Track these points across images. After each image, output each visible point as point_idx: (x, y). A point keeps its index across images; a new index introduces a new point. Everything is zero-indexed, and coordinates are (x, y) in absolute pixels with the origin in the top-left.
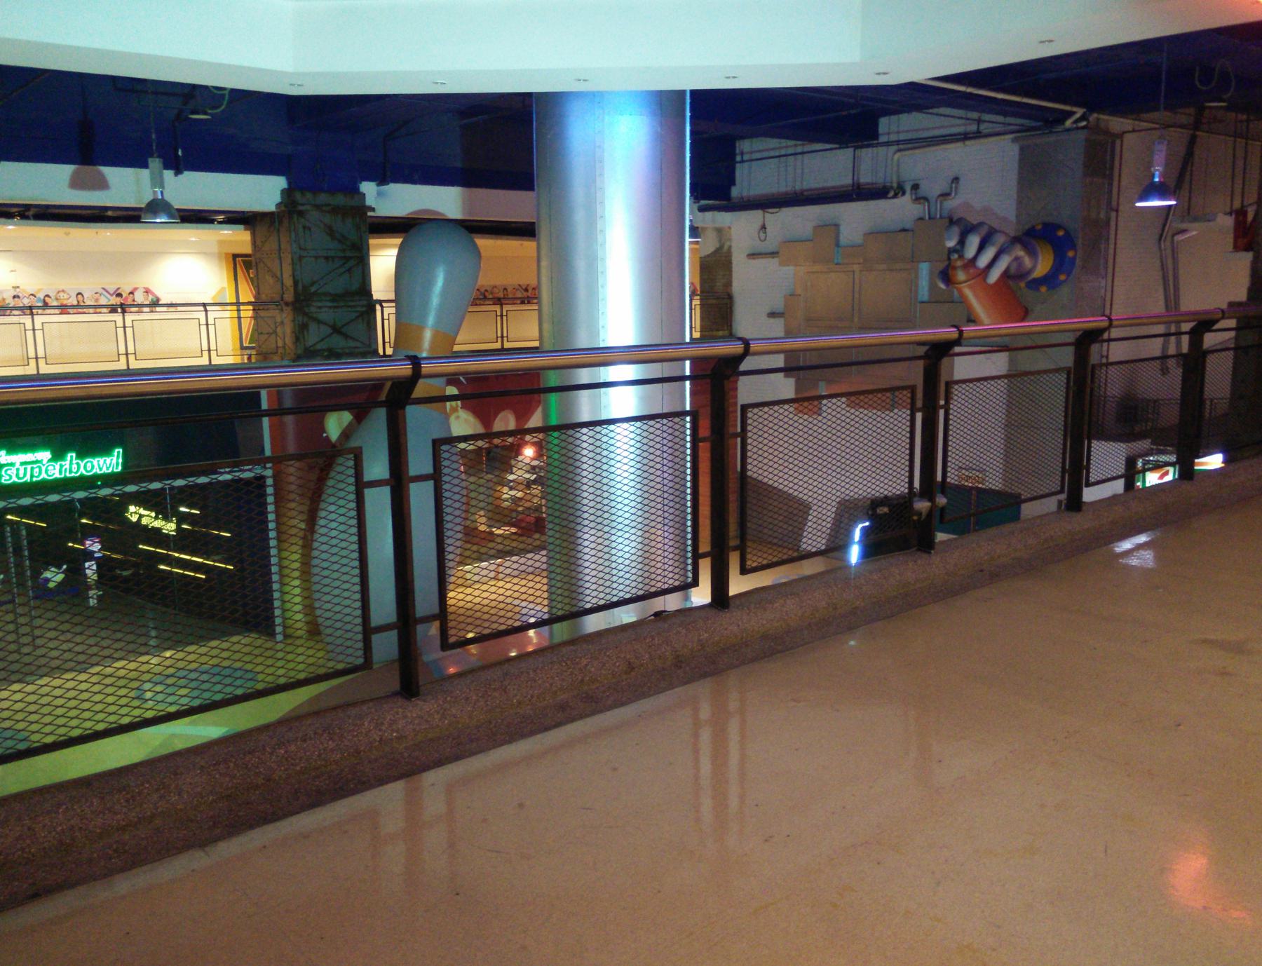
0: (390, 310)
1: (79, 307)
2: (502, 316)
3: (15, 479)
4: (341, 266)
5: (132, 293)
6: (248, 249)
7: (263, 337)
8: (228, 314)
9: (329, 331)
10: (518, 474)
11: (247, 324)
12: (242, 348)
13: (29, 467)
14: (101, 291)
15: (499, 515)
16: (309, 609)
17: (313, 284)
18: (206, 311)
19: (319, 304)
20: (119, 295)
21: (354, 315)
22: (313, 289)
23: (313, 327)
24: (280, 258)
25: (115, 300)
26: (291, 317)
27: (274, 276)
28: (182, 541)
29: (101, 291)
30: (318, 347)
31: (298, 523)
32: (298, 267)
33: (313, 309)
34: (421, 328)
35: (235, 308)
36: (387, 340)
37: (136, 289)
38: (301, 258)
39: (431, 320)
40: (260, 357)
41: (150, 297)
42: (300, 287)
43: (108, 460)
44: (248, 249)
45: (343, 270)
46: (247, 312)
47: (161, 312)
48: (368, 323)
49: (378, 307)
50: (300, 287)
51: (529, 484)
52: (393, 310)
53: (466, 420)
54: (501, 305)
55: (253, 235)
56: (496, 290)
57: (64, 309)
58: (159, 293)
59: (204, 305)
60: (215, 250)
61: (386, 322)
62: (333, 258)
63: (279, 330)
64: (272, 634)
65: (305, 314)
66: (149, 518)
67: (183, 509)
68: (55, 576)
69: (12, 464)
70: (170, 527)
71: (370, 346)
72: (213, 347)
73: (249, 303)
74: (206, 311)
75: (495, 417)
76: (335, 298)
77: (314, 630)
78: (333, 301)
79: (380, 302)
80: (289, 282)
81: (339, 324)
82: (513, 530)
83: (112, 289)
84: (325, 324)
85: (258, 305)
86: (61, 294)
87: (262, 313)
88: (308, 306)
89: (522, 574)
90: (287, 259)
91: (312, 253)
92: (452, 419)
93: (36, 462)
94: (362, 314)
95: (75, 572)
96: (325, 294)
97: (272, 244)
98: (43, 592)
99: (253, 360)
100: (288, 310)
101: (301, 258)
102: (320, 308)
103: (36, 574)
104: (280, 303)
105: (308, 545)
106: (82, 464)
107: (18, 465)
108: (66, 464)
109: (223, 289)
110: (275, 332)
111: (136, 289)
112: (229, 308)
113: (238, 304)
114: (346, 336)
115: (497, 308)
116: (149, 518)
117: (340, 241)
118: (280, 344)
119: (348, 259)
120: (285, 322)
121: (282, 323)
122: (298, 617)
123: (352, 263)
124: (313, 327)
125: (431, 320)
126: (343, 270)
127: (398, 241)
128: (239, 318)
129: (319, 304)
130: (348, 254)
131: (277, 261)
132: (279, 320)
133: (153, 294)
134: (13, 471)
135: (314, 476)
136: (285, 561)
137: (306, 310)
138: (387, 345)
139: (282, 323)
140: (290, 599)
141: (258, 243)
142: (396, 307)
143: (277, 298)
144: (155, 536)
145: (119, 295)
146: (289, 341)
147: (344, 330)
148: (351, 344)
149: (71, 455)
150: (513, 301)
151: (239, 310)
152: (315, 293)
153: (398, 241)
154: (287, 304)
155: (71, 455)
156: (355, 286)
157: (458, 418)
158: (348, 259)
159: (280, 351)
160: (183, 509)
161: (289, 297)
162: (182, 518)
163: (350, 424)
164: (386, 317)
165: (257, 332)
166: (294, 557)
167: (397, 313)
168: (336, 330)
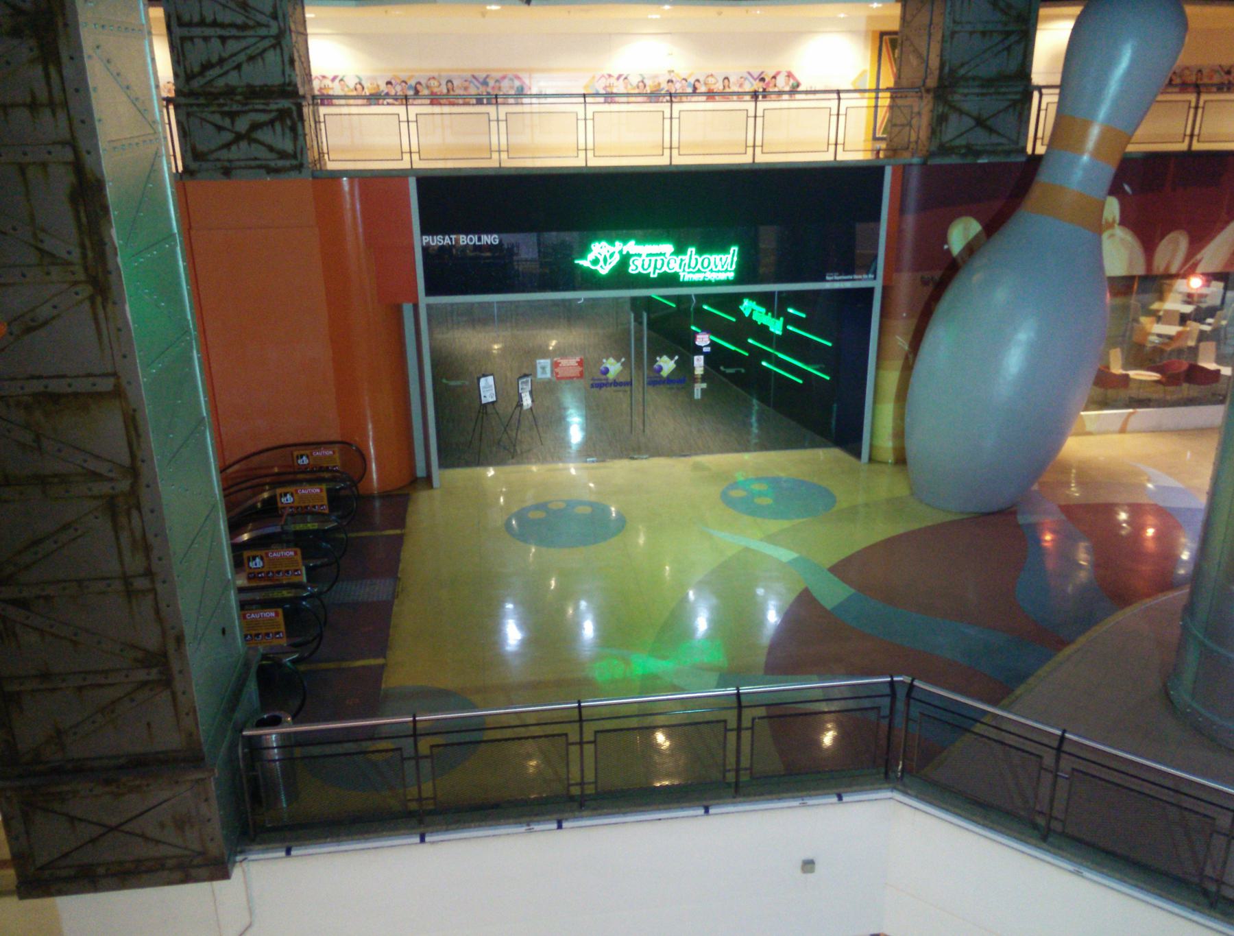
0: (1051, 99)
1: (725, 95)
2: (1197, 108)
3: (640, 270)
4: (1002, 41)
5: (774, 77)
6: (895, 26)
7: (896, 129)
8: (864, 103)
9: (971, 123)
10: (1173, 304)
11: (883, 113)
12: (875, 139)
13: (653, 259)
14: (471, 79)
15: (1140, 355)
16: (900, 434)
17: (962, 65)
18: (839, 99)
19: (966, 91)
20: (763, 80)
21: (1006, 104)
22: (962, 72)
23: (953, 117)
24: (930, 35)
25: (759, 86)
26: (930, 107)
27: (920, 56)
28: (787, 342)
29: (471, 79)
30: (957, 142)
31: (901, 342)
32: (948, 45)
33: (957, 97)
34: (1087, 124)
35: (873, 95)
36: (1040, 134)
37: (778, 73)
38: (953, 33)
39: (1103, 113)
40: (890, 153)
41: (792, 81)
42: (947, 69)
43: (724, 256)
44: (895, 26)
45: (1000, 47)
46: (885, 101)
47: (800, 102)
48: (1020, 114)
49: (1036, 94)
50: (947, 69)
51: (1183, 319)
52: (1056, 99)
53: (1122, 240)
54: (1199, 93)
55: (904, 7)
56: (434, 83)
57: (711, 95)
58: (800, 77)
59: (838, 92)
60: (862, 26)
61: (1042, 114)
62: (991, 32)
63: (914, 122)
64: (857, 454)
65: (947, 103)
66: (761, 315)
67: (791, 310)
68: (667, 365)
69: (639, 255)
70: (776, 326)
71: (1017, 143)
72: (840, 140)
73: (888, 89)
74: (839, 99)
75: (1163, 237)
76: (988, 83)
77: (901, 460)
78: (982, 86)
79: (1039, 88)
80: (934, 62)
81: (985, 115)
82: (1154, 376)
83: (756, 74)
84: (968, 115)
85: (896, 92)
86: (710, 79)
87: (900, 102)
88: (1161, 298)
89: (1157, 430)
90: (937, 36)
91: (969, 28)
92: (1105, 236)
93: (660, 254)
94: (1014, 104)
95: (685, 366)
96: (974, 78)
97: (923, 18)
98: (657, 380)
99: (881, 155)
100: (929, 98)
101: (953, 33)
102: (965, 95)
103: (652, 361)
104: (921, 89)
105: (908, 368)
106: (700, 260)
107: (644, 257)
108: (686, 258)
109: (864, 72)
110: (910, 124)
111: (778, 73)
112: (867, 95)
113: (877, 90)
114: (991, 130)
115: (1192, 98)
116: (761, 315)
117: (1002, 11)
118: (913, 138)
119: (1008, 34)
120: (924, 108)
121: (919, 114)
122: (886, 442)
123: (1013, 38)
124: (953, 117)
125: (1103, 113)
126: (1000, 47)
127: (1077, 10)
128: (876, 107)
129: (966, 91)
130: (1011, 28)
131: (926, 38)
132: (916, 110)
133: (794, 78)
134: (639, 262)
135: (927, 291)
136: (882, 380)
137: (950, 98)
138: (1039, 142)
139: (919, 114)
140: (881, 420)
141: (908, 18)
142: (1061, 95)
143: (919, 83)
144: (762, 332)
145: (763, 80)
146: (924, 134)
147: (989, 123)
148: (995, 139)
149: (692, 250)
150: (1208, 88)
151: (877, 98)
152: (964, 78)
153: (1077, 10)
154: (928, 91)
155: (692, 250)
156: (1013, 66)
157: (1112, 236)
158: (1008, 34)
159: (912, 146)
160: (791, 310)
161: (932, 82)
162: (790, 319)
163: (976, 237)
164: (1043, 106)
165: (891, 124)
166: (891, 378)
167: (1060, 105)
168: (980, 122)
